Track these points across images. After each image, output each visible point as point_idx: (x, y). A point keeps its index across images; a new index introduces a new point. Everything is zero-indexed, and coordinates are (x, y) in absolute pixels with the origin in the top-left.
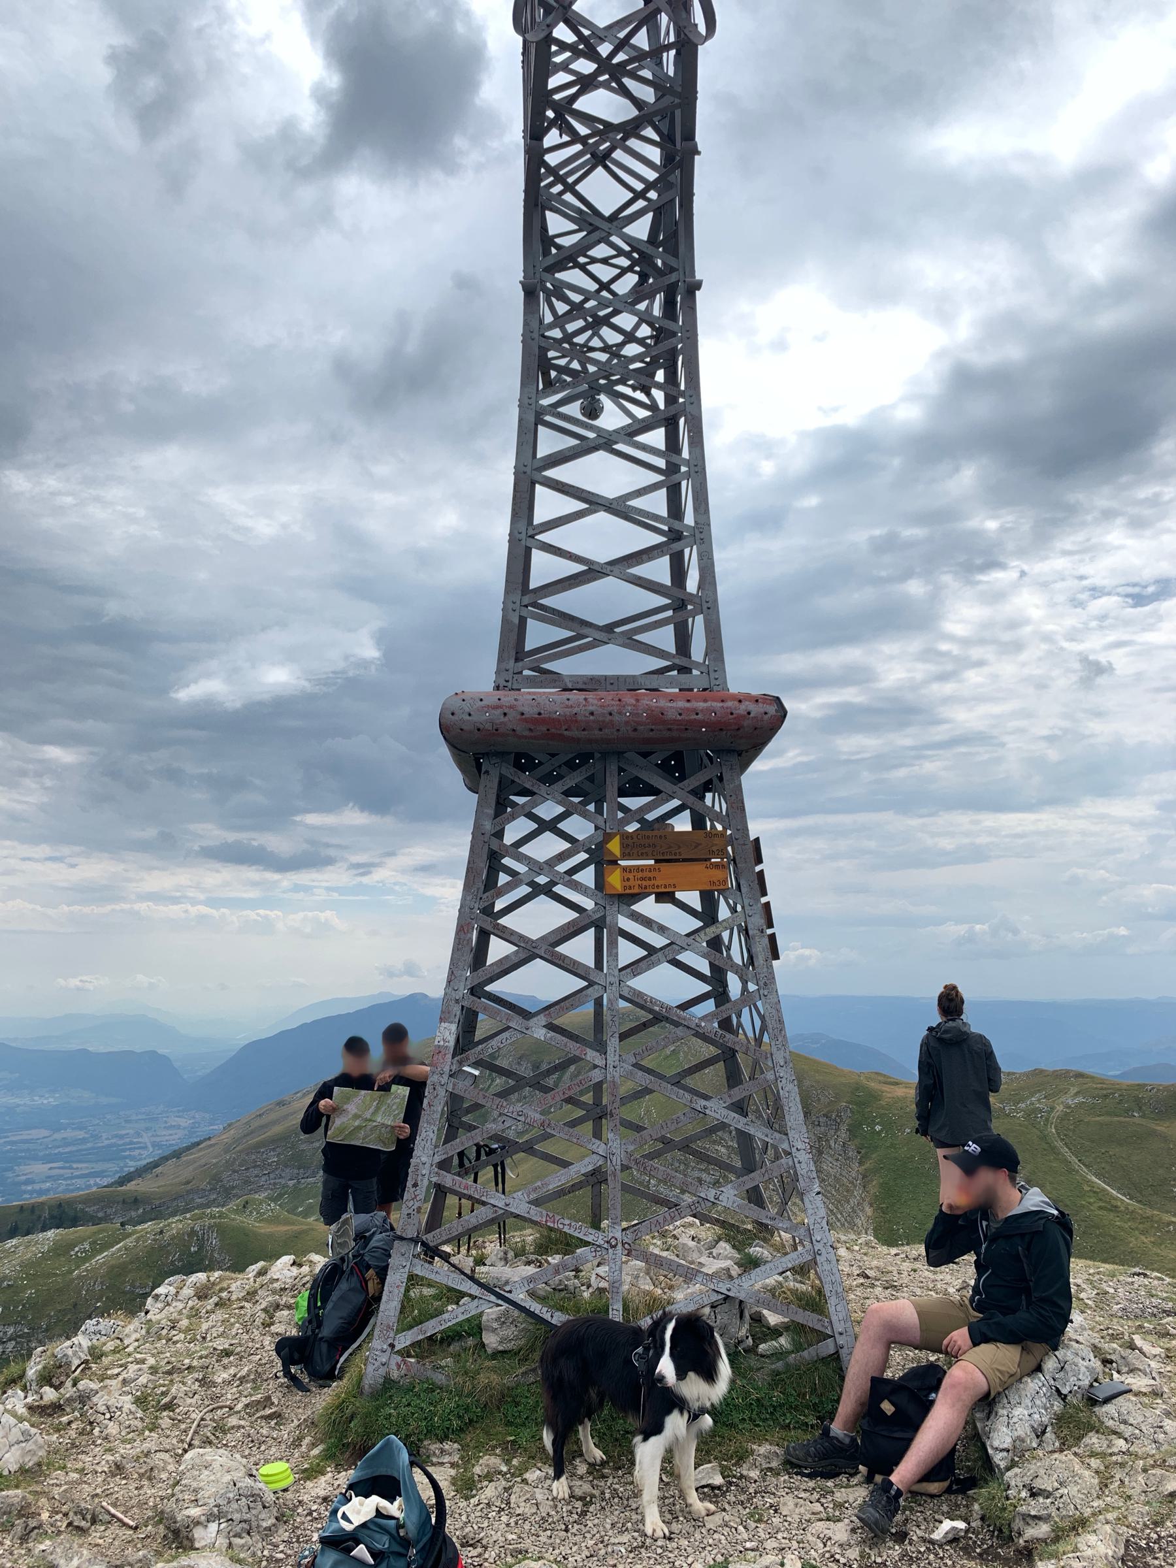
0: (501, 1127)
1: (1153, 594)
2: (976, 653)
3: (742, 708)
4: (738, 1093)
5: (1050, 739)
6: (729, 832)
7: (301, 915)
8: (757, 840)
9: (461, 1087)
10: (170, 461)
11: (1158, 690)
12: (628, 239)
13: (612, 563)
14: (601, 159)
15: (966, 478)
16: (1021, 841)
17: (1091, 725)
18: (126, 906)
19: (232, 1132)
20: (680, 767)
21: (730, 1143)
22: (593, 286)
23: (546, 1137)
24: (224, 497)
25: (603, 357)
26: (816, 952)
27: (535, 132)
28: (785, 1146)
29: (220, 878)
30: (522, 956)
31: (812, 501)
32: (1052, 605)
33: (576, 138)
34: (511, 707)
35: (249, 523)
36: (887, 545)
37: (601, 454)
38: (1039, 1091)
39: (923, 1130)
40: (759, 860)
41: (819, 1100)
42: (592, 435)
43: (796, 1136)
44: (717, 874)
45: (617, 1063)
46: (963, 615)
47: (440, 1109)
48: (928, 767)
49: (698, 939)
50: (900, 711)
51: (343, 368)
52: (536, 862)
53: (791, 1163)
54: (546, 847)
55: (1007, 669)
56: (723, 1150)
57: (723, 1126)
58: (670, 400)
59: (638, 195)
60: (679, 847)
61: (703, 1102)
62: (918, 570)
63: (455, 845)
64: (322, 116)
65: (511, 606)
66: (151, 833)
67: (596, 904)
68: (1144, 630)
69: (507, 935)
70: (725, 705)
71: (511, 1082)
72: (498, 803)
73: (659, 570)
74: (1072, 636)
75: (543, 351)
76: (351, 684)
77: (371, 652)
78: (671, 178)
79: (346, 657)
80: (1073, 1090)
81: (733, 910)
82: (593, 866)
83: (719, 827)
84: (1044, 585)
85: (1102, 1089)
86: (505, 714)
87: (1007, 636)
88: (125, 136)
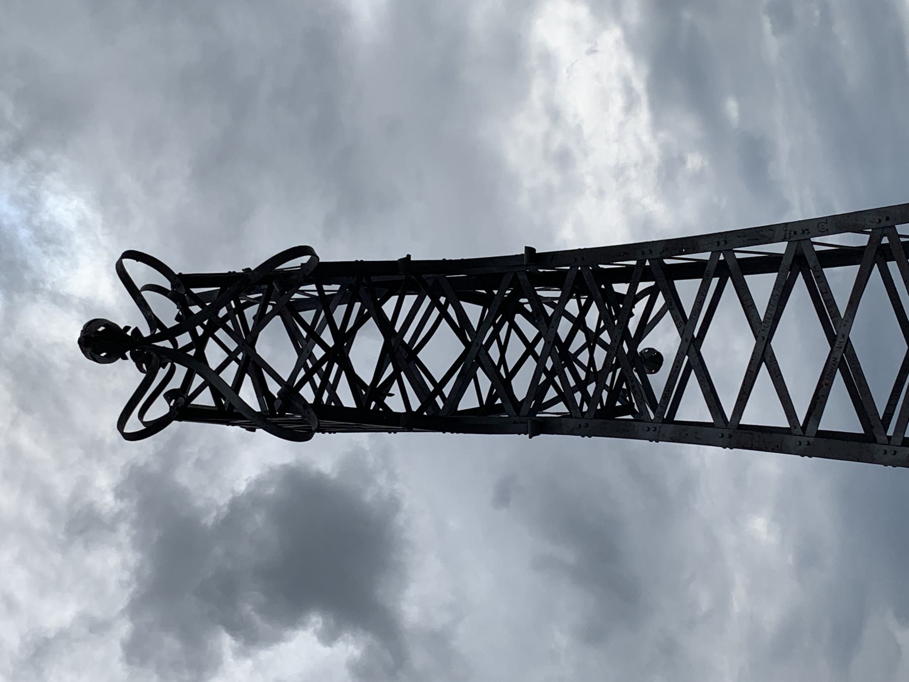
13: (832, 338)
22: (531, 364)
31: (732, 108)
33: (395, 376)
51: (593, 635)
59: (444, 315)
64: (347, 635)
73: (840, 279)
75: (598, 415)
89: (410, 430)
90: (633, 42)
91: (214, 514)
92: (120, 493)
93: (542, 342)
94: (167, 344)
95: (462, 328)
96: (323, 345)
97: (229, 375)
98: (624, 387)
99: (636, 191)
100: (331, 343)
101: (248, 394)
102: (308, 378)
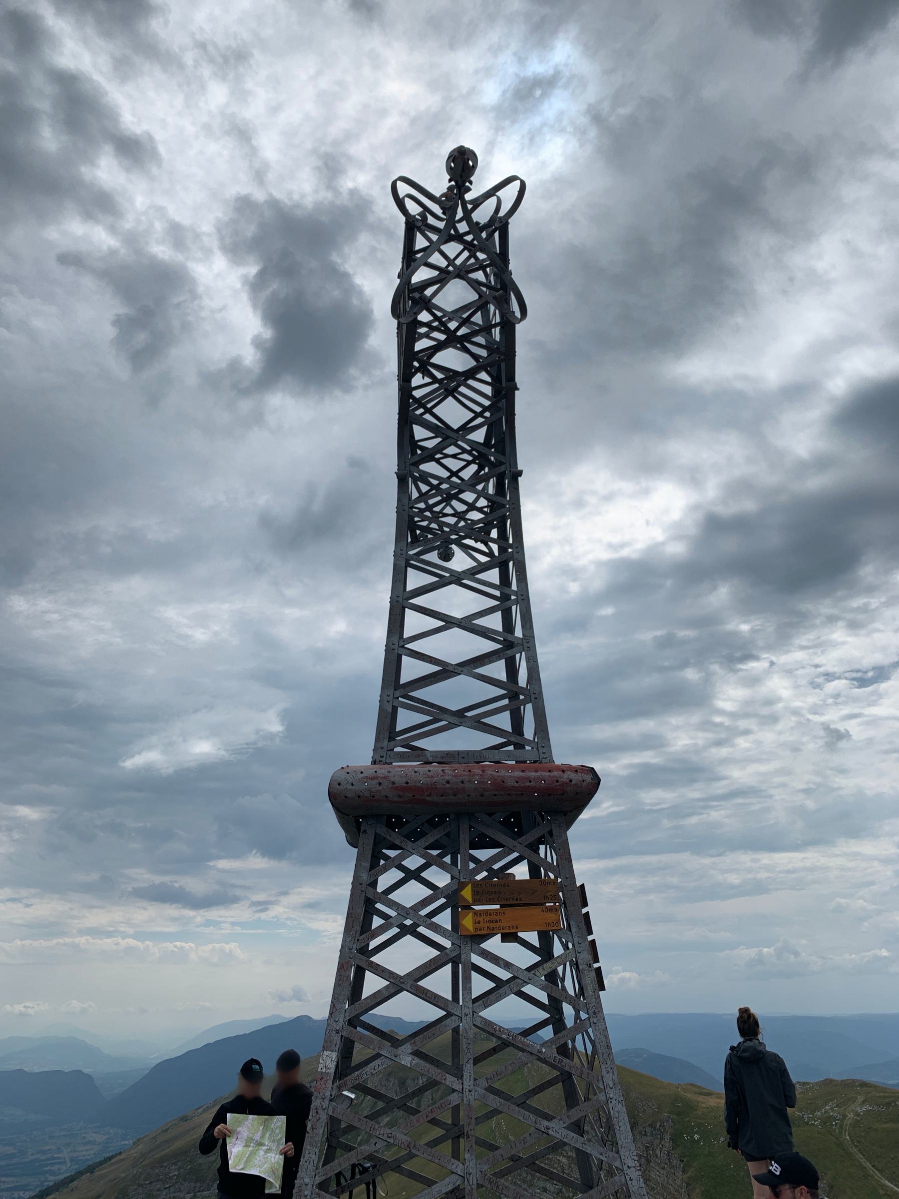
0: (373, 1148)
1: (872, 677)
2: (742, 724)
3: (566, 777)
4: (575, 1114)
5: (807, 792)
6: (559, 880)
7: (210, 946)
8: (582, 886)
9: (340, 1110)
10: (136, 587)
11: (887, 752)
12: (472, 443)
13: (462, 665)
14: (451, 392)
15: (721, 595)
16: (793, 876)
17: (837, 780)
18: (67, 940)
19: (140, 1147)
20: (518, 823)
21: (570, 1154)
22: (445, 474)
23: (411, 1156)
24: (171, 613)
25: (452, 520)
26: (635, 975)
27: (405, 376)
28: (617, 1164)
29: (146, 914)
30: (392, 991)
32: (797, 687)
33: (435, 380)
34: (385, 778)
35: (189, 632)
36: (666, 643)
37: (453, 587)
38: (831, 1100)
39: (734, 1144)
40: (585, 904)
41: (644, 1111)
42: (447, 575)
43: (627, 1154)
44: (551, 917)
45: (472, 1087)
46: (730, 696)
47: (321, 1131)
48: (715, 815)
49: (537, 974)
50: (687, 770)
51: (266, 521)
52: (404, 907)
53: (623, 1180)
54: (411, 894)
55: (768, 736)
56: (564, 1160)
57: (563, 1144)
58: (502, 550)
59: (477, 415)
60: (520, 894)
61: (546, 1123)
62: (692, 661)
63: (339, 884)
65: (386, 698)
66: (94, 877)
67: (453, 944)
68: (869, 705)
69: (380, 971)
70: (552, 774)
71: (381, 1105)
72: (373, 856)
73: (498, 670)
74: (815, 710)
75: (411, 518)
76: (259, 753)
77: (276, 727)
78: (500, 405)
79: (257, 732)
80: (860, 1099)
81: (566, 947)
82: (450, 909)
83: (552, 876)
84: (789, 672)
85: (884, 1097)
86: (380, 784)
87: (765, 711)
88: (120, 369)
89: (400, 389)
90: (654, 549)
91: (339, 261)
92: (353, 192)
93: (459, 482)
94: (460, 214)
95: (466, 428)
96: (458, 329)
97: (436, 259)
98: (430, 536)
99: (556, 551)
100: (459, 333)
101: (422, 275)
102: (436, 318)
